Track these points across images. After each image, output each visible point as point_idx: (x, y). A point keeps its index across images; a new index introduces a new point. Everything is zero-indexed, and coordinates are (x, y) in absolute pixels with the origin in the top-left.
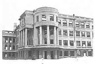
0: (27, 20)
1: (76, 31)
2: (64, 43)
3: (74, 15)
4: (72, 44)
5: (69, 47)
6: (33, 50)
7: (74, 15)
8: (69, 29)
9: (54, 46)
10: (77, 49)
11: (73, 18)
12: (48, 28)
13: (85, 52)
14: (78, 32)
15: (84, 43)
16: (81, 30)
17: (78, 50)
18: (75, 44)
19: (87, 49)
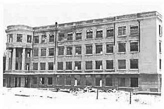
0: (142, 29)
1: (59, 47)
2: (67, 66)
3: (56, 23)
4: (51, 68)
5: (47, 72)
6: (114, 76)
7: (56, 23)
8: (104, 41)
9: (114, 71)
10: (57, 75)
11: (55, 28)
12: (24, 50)
13: (123, 79)
14: (61, 49)
15: (43, 65)
16: (93, 42)
17: (58, 76)
18: (55, 67)
19: (72, 75)
